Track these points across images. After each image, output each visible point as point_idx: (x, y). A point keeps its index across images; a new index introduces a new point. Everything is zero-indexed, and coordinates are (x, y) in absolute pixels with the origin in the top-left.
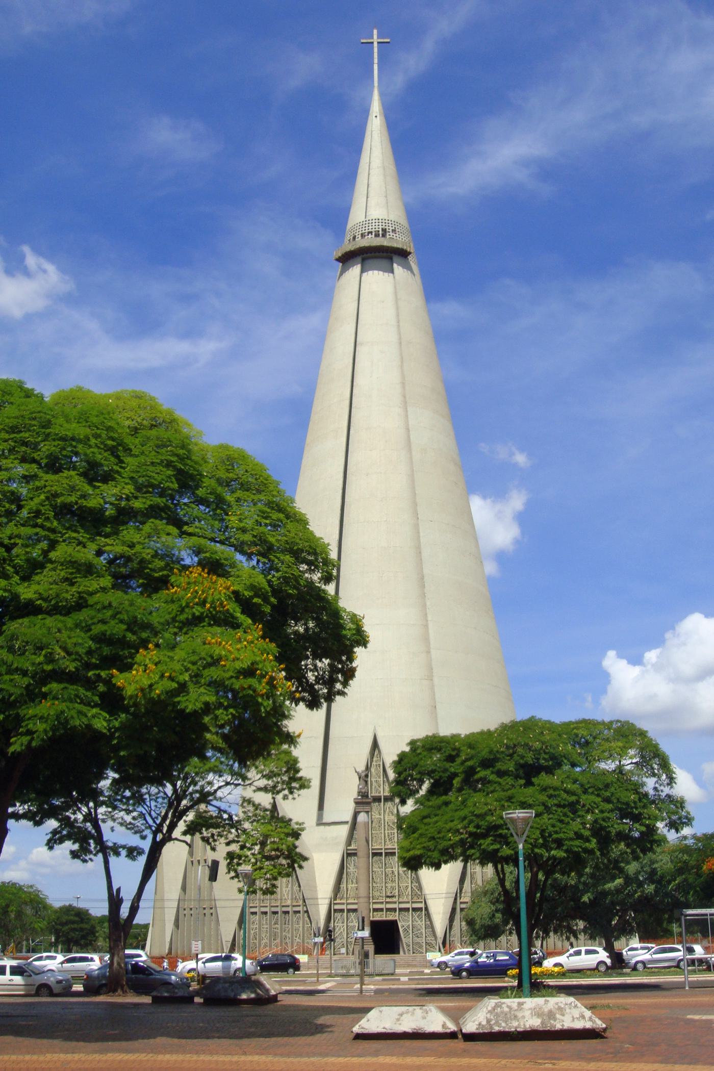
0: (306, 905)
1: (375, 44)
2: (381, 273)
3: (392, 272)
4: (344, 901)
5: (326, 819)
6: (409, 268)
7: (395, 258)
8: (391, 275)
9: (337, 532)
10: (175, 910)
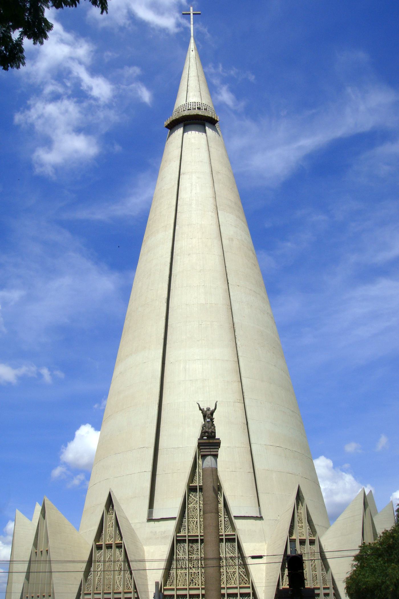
0: (136, 592)
1: (192, 14)
2: (197, 132)
3: (205, 132)
4: (174, 587)
5: (155, 516)
6: (216, 131)
7: (206, 124)
8: (204, 134)
9: (166, 292)
10: (20, 595)
